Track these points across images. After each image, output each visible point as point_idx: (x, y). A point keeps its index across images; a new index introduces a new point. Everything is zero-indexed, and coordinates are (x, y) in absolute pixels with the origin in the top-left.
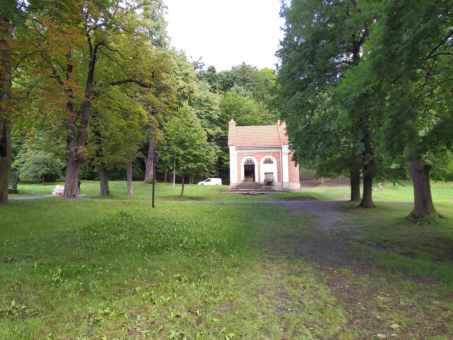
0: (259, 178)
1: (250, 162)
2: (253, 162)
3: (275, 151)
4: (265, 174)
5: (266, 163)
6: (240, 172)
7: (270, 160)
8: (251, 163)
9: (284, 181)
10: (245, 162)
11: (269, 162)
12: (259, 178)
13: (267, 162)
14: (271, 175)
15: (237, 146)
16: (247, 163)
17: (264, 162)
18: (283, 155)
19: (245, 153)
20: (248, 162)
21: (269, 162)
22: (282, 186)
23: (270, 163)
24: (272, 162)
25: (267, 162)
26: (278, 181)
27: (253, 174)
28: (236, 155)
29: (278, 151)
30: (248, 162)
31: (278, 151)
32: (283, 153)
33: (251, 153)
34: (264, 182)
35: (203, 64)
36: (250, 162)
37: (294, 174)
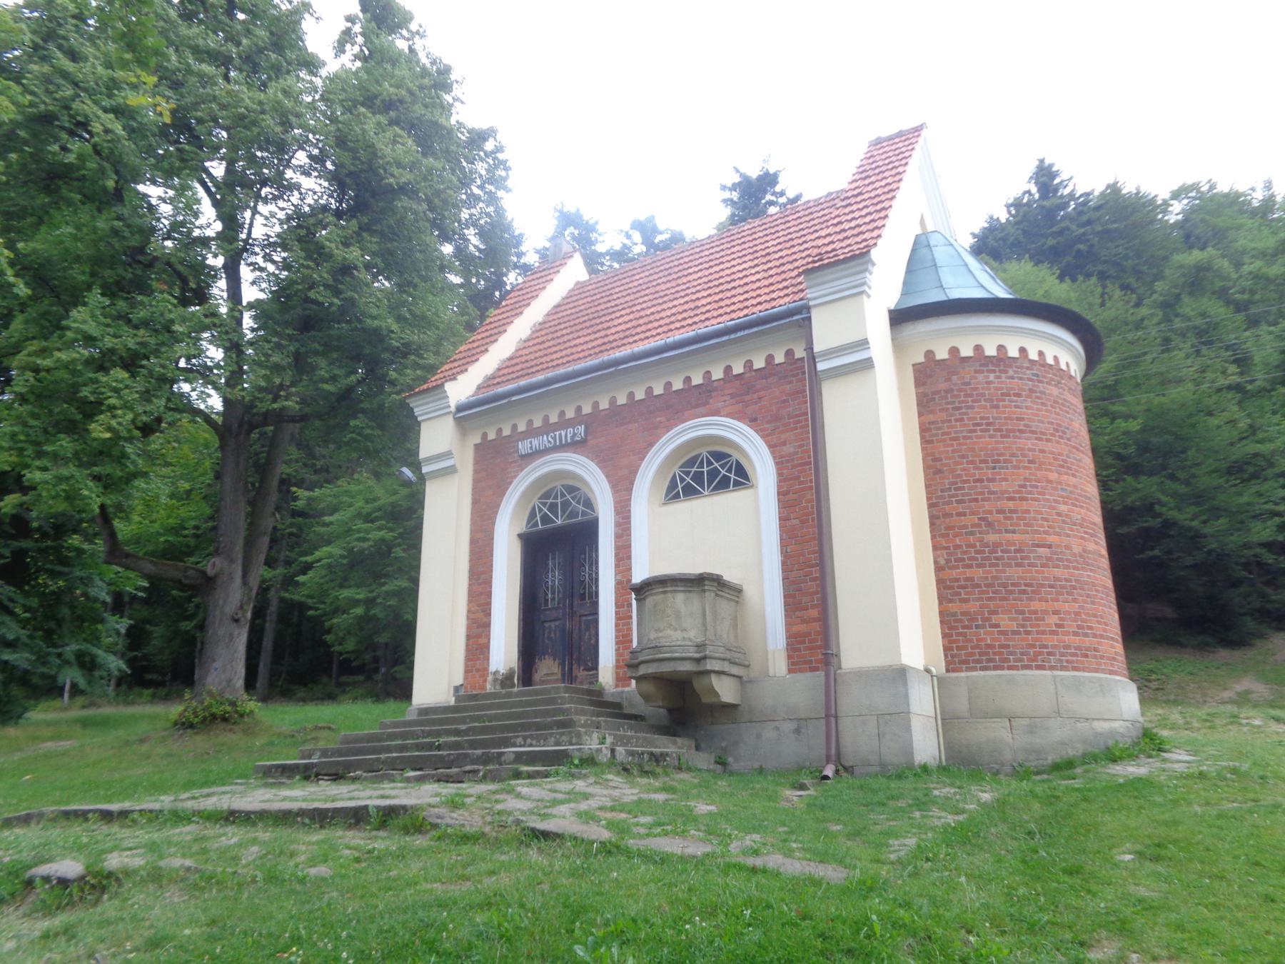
1: (566, 504)
3: (718, 374)
5: (690, 492)
7: (719, 456)
11: (713, 474)
13: (698, 477)
16: (545, 519)
17: (673, 485)
19: (531, 433)
23: (723, 485)
29: (780, 358)
36: (553, 508)
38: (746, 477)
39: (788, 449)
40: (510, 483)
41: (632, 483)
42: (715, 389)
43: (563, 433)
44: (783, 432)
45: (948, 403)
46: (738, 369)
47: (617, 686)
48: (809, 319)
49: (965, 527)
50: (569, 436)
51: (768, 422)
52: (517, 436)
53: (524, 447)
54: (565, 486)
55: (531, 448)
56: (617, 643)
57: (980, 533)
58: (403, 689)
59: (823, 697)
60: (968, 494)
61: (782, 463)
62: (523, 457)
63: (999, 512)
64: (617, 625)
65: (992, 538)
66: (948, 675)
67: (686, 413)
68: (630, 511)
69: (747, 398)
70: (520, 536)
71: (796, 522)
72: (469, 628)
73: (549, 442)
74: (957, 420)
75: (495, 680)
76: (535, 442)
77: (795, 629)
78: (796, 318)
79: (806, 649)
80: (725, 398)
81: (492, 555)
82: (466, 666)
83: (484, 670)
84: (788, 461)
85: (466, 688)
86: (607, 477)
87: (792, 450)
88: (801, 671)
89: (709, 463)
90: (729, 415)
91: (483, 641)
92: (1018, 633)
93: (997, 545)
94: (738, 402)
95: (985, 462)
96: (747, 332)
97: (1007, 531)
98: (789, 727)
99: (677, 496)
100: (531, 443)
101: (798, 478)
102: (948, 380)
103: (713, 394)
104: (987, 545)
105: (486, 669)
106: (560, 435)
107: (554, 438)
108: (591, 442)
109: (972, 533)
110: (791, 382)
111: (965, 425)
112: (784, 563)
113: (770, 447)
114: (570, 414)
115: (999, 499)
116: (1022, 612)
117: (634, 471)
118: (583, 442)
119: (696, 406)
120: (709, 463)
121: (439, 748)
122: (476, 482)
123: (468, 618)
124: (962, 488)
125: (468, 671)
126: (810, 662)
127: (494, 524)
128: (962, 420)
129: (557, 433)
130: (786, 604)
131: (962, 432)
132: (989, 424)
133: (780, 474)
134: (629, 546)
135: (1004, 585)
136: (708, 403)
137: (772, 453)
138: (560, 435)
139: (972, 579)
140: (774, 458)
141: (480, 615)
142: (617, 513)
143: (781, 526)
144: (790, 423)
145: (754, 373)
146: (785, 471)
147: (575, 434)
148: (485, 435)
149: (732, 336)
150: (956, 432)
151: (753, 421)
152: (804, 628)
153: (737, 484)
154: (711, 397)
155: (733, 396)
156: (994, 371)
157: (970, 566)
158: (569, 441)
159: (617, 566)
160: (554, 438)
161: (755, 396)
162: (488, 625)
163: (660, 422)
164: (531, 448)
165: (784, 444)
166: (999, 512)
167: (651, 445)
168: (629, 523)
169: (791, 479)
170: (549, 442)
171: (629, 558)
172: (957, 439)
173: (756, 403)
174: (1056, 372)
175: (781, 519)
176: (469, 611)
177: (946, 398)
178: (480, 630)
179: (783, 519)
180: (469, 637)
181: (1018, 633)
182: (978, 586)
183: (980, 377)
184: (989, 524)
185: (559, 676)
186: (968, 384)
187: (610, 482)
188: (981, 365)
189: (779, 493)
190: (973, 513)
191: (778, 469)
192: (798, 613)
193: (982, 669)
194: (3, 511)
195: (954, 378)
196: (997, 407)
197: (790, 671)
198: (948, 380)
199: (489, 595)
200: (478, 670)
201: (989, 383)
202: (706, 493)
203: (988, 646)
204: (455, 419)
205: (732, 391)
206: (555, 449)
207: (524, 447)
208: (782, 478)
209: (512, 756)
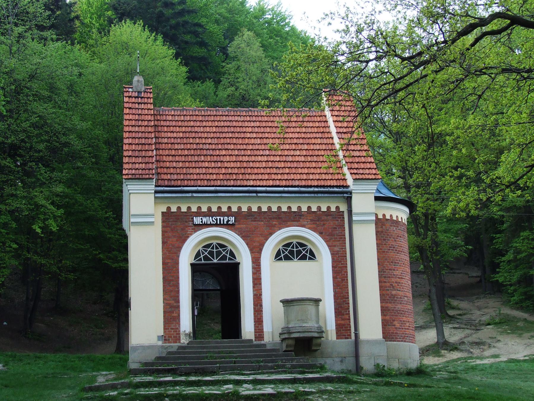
0: (258, 321)
1: (219, 253)
2: (232, 254)
3: (304, 209)
4: (286, 303)
5: (287, 258)
6: (177, 299)
7: (302, 245)
8: (224, 258)
9: (364, 335)
10: (198, 255)
11: (299, 252)
12: (258, 321)
13: (291, 252)
14: (311, 308)
15: (160, 182)
16: (206, 258)
17: (278, 254)
18: (355, 227)
19: (199, 213)
20: (211, 253)
22: (357, 356)
23: (304, 258)
24: (312, 253)
25: (291, 252)
26: (339, 336)
27: (196, 313)
28: (158, 220)
29: (333, 209)
30: (211, 253)
31: (333, 209)
32: (354, 218)
33: (224, 214)
34: (278, 339)
35: (291, 17)
36: (219, 253)
37: (399, 307)
38: (314, 256)
39: (336, 249)
40: (188, 237)
41: (261, 250)
42: (303, 215)
43: (222, 219)
44: (334, 241)
45: (382, 237)
46: (314, 209)
47: (255, 340)
48: (351, 197)
51: (328, 235)
52: (189, 214)
53: (197, 220)
54: (218, 244)
55: (202, 222)
56: (255, 322)
57: (391, 290)
59: (353, 349)
60: (387, 275)
62: (195, 225)
63: (396, 282)
64: (254, 314)
65: (394, 292)
66: (338, 340)
67: (289, 223)
68: (260, 263)
69: (318, 223)
70: (192, 265)
71: (340, 280)
72: (164, 307)
73: (213, 221)
74: (384, 244)
76: (205, 220)
77: (339, 322)
79: (343, 330)
80: (308, 220)
81: (178, 272)
82: (164, 326)
83: (177, 330)
84: (336, 254)
85: (165, 337)
86: (247, 244)
87: (338, 250)
88: (341, 338)
89: (307, 252)
90: (309, 228)
91: (175, 314)
92: (400, 328)
94: (314, 224)
95: (392, 262)
97: (398, 290)
98: (337, 360)
99: (281, 259)
100: (202, 219)
101: (341, 262)
102: (382, 227)
104: (392, 295)
106: (220, 219)
107: (217, 220)
108: (237, 226)
110: (338, 220)
111: (387, 247)
112: (334, 296)
113: (329, 246)
114: (224, 209)
116: (401, 321)
117: (262, 245)
118: (233, 225)
119: (294, 221)
120: (307, 252)
121: (252, 363)
122: (164, 232)
123: (164, 303)
125: (165, 329)
126: (345, 335)
127: (178, 257)
128: (386, 244)
129: (218, 218)
130: (335, 312)
131: (386, 249)
132: (394, 248)
133: (333, 259)
134: (261, 279)
135: (397, 311)
136: (299, 221)
138: (220, 219)
140: (330, 252)
141: (172, 302)
142: (253, 262)
143: (334, 281)
144: (337, 238)
145: (321, 213)
146: (335, 258)
147: (228, 221)
148: (169, 208)
149: (316, 195)
150: (384, 249)
151: (321, 234)
152: (343, 322)
153: (310, 259)
155: (311, 220)
156: (395, 226)
157: (387, 303)
159: (254, 287)
160: (217, 220)
162: (178, 307)
163: (275, 224)
164: (202, 222)
165: (335, 246)
166: (396, 282)
167: (271, 234)
168: (260, 268)
169: (337, 262)
170: (213, 221)
171: (260, 284)
172: (384, 252)
173: (322, 226)
174: (396, 223)
176: (164, 299)
177: (381, 235)
178: (173, 309)
179: (334, 278)
180: (165, 312)
181: (400, 328)
183: (392, 228)
184: (393, 287)
186: (388, 230)
187: (249, 247)
188: (392, 223)
189: (333, 267)
190: (388, 282)
191: (332, 257)
192: (340, 316)
193: (390, 341)
196: (396, 241)
197: (337, 338)
198: (382, 227)
199: (178, 292)
200: (172, 329)
201: (394, 231)
202: (295, 260)
204: (155, 197)
205: (311, 218)
206: (216, 225)
207: (197, 220)
208: (334, 261)
209: (290, 366)
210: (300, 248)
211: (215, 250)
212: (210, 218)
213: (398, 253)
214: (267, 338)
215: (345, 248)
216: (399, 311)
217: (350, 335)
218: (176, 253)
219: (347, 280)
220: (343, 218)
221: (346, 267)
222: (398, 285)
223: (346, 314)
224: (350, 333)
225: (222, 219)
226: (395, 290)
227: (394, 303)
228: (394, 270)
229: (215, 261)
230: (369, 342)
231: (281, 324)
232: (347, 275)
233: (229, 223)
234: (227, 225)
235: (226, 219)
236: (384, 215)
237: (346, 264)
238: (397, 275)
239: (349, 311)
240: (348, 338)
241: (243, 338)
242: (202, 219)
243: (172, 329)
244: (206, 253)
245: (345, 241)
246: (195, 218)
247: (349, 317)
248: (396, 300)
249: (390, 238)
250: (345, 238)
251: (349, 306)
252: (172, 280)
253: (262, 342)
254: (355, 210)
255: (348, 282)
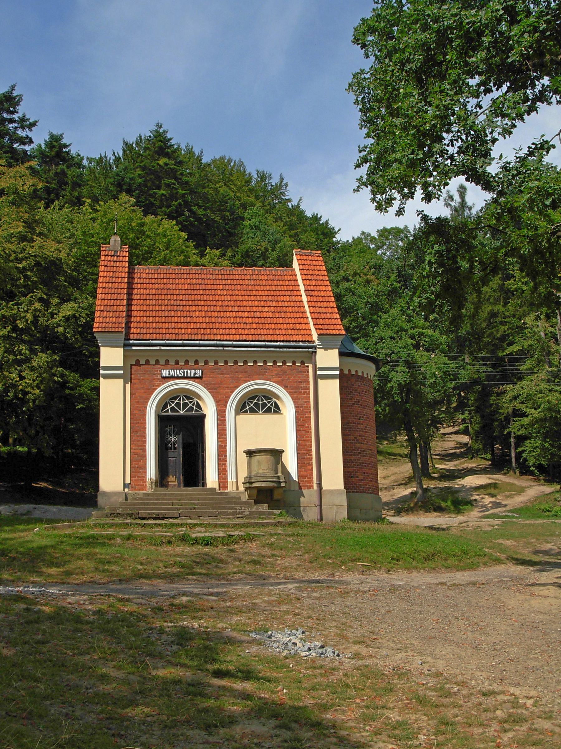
2: (198, 406)
4: (250, 453)
9: (326, 486)
10: (165, 406)
13: (256, 405)
17: (244, 406)
21: (264, 405)
22: (321, 506)
23: (269, 410)
24: (277, 406)
25: (256, 405)
42: (269, 369)
47: (219, 490)
48: (316, 352)
49: (350, 440)
50: (192, 374)
55: (169, 374)
58: (204, 485)
61: (298, 407)
65: (358, 445)
69: (283, 377)
73: (180, 374)
75: (152, 483)
76: (172, 372)
78: (310, 350)
83: (143, 478)
90: (274, 382)
92: (362, 480)
93: (359, 448)
95: (356, 416)
96: (288, 350)
99: (246, 411)
100: (169, 372)
102: (347, 382)
103: (268, 371)
104: (356, 448)
105: (145, 477)
106: (187, 372)
107: (184, 372)
109: (352, 443)
115: (360, 431)
118: (200, 378)
124: (350, 426)
129: (186, 371)
137: (294, 402)
138: (187, 372)
139: (351, 460)
140: (295, 405)
147: (195, 374)
149: (281, 350)
151: (285, 387)
153: (275, 411)
154: (266, 372)
155: (277, 374)
158: (192, 376)
161: (287, 376)
164: (169, 374)
166: (360, 436)
170: (180, 374)
175: (296, 430)
178: (139, 458)
181: (362, 480)
182: (353, 462)
184: (357, 440)
185: (176, 483)
186: (353, 385)
190: (353, 436)
194: (558, 487)
195: (349, 382)
198: (347, 382)
200: (139, 477)
201: (359, 386)
203: (355, 484)
206: (183, 378)
210: (265, 401)
211: (182, 402)
212: (178, 371)
213: (362, 408)
214: (231, 488)
215: (310, 402)
216: (363, 463)
217: (312, 486)
218: (143, 404)
219: (311, 432)
220: (308, 372)
221: (310, 420)
222: (362, 439)
223: (309, 465)
224: (313, 483)
225: (189, 372)
226: (359, 443)
227: (357, 455)
228: (358, 424)
229: (182, 412)
230: (331, 492)
231: (243, 474)
232: (311, 427)
233: (197, 376)
234: (194, 378)
235: (193, 372)
236: (350, 371)
237: (310, 417)
238: (362, 429)
239: (312, 463)
240: (310, 488)
241: (208, 487)
242: (169, 372)
243: (139, 477)
244: (260, 402)
245: (309, 394)
246: (162, 371)
247: (312, 468)
248: (359, 453)
249: (355, 392)
250: (309, 392)
251: (312, 458)
252: (140, 431)
253: (226, 491)
254: (318, 365)
255: (311, 435)
